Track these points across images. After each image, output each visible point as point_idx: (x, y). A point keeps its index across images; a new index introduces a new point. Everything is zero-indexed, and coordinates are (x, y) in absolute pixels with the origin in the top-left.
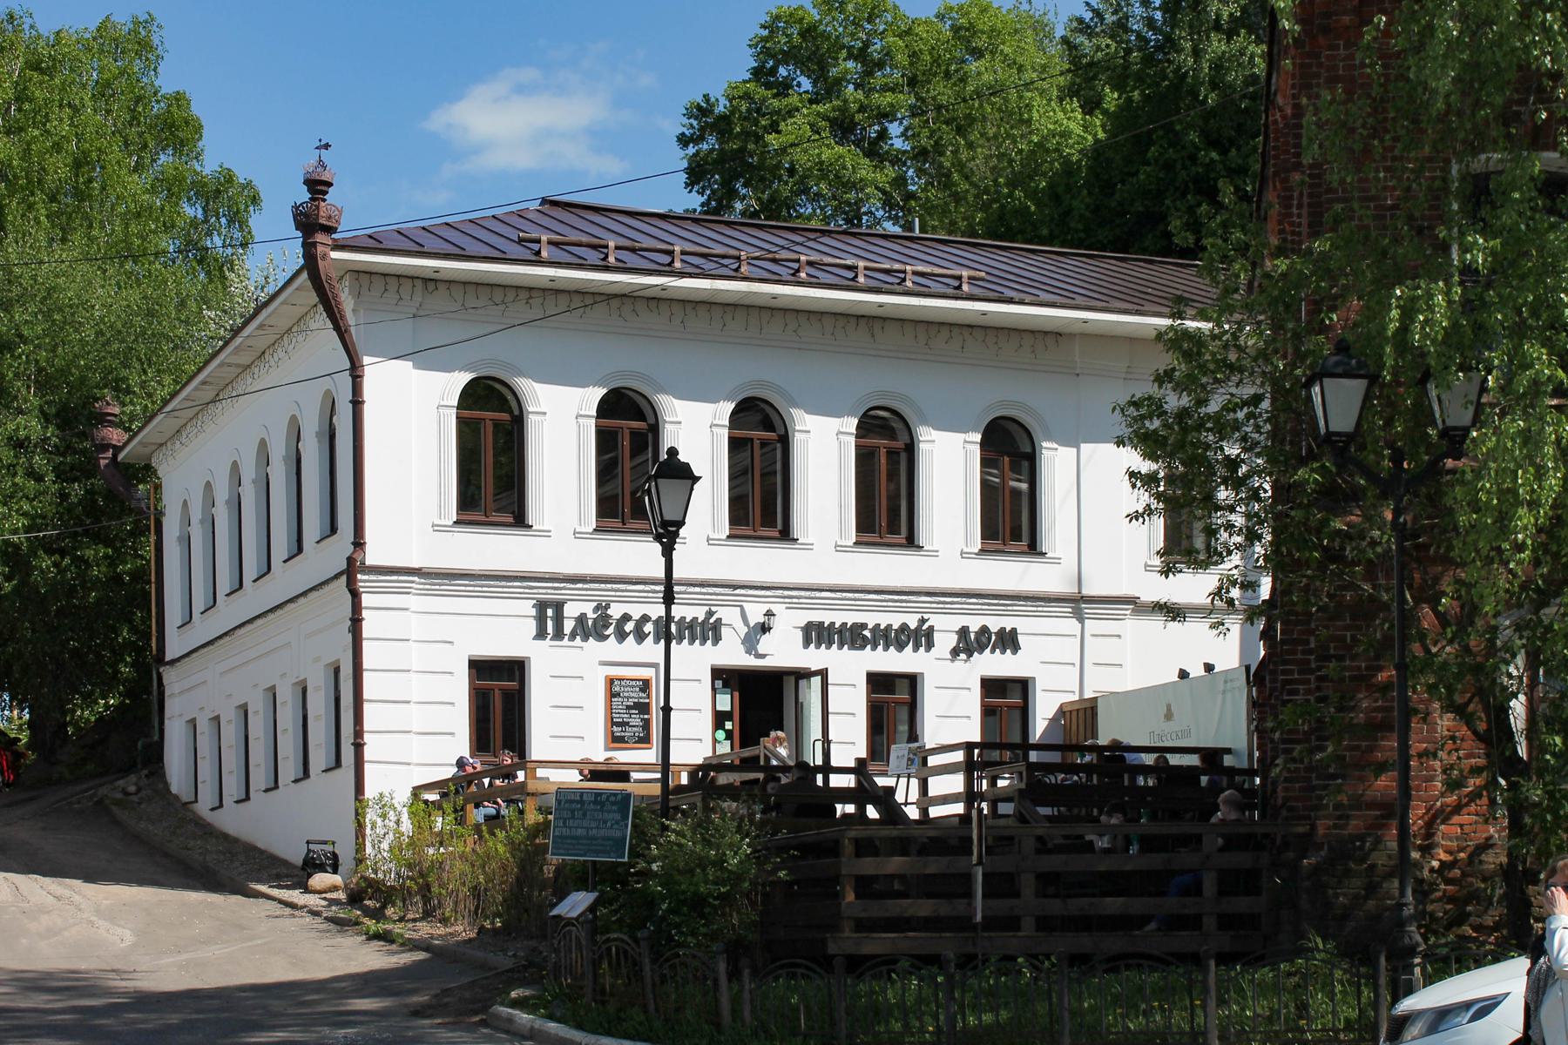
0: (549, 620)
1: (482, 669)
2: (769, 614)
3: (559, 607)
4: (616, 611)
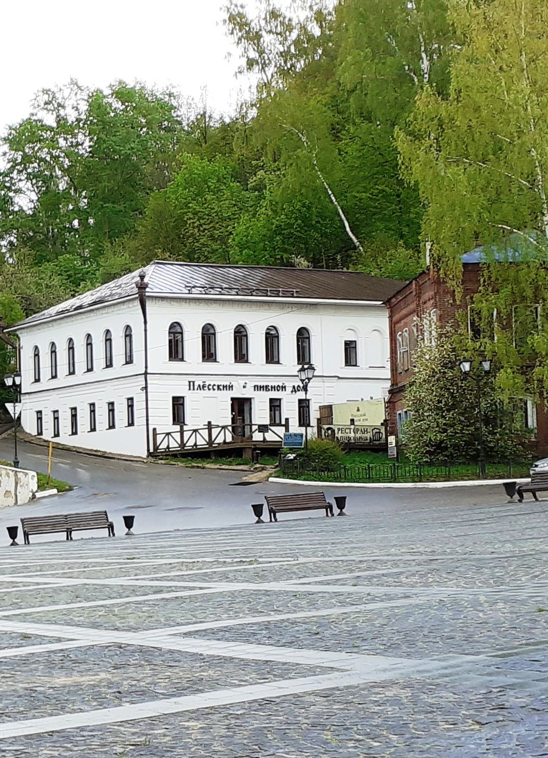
0: (191, 385)
1: (175, 399)
2: (246, 383)
3: (194, 382)
4: (207, 384)
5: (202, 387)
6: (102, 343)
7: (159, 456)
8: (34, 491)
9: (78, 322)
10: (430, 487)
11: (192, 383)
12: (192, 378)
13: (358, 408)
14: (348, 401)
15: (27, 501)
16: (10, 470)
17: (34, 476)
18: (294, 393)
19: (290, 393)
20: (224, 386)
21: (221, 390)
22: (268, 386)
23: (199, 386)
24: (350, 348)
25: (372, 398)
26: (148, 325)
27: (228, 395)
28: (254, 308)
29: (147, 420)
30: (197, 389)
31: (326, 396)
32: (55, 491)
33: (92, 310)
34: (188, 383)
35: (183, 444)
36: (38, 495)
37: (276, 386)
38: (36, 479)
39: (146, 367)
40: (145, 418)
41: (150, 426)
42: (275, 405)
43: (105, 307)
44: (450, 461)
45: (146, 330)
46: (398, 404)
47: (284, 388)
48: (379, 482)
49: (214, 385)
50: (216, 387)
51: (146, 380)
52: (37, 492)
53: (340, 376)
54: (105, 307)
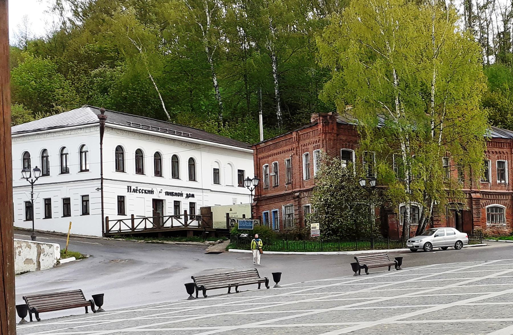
0: (129, 189)
3: (131, 187)
5: (135, 191)
6: (39, 158)
7: (114, 235)
8: (58, 259)
9: (60, 137)
10: (348, 254)
11: (129, 188)
12: (129, 184)
13: (231, 209)
14: (215, 205)
15: (52, 266)
16: (32, 242)
17: (58, 247)
18: (187, 198)
19: (185, 198)
20: (148, 191)
21: (147, 193)
22: (173, 193)
23: (134, 190)
24: (216, 172)
25: (241, 203)
26: (103, 145)
27: (150, 198)
28: (166, 141)
29: (103, 211)
30: (133, 192)
31: (204, 201)
32: (73, 259)
33: (50, 133)
34: (127, 188)
35: (133, 228)
36: (62, 261)
37: (188, 194)
38: (59, 249)
39: (102, 175)
40: (101, 209)
41: (104, 215)
42: (177, 205)
43: (63, 131)
44: (343, 239)
45: (101, 149)
46: (261, 208)
47: (181, 195)
48: (312, 251)
49: (143, 190)
50: (143, 191)
51: (102, 183)
52: (60, 259)
53: (212, 190)
54: (63, 131)
